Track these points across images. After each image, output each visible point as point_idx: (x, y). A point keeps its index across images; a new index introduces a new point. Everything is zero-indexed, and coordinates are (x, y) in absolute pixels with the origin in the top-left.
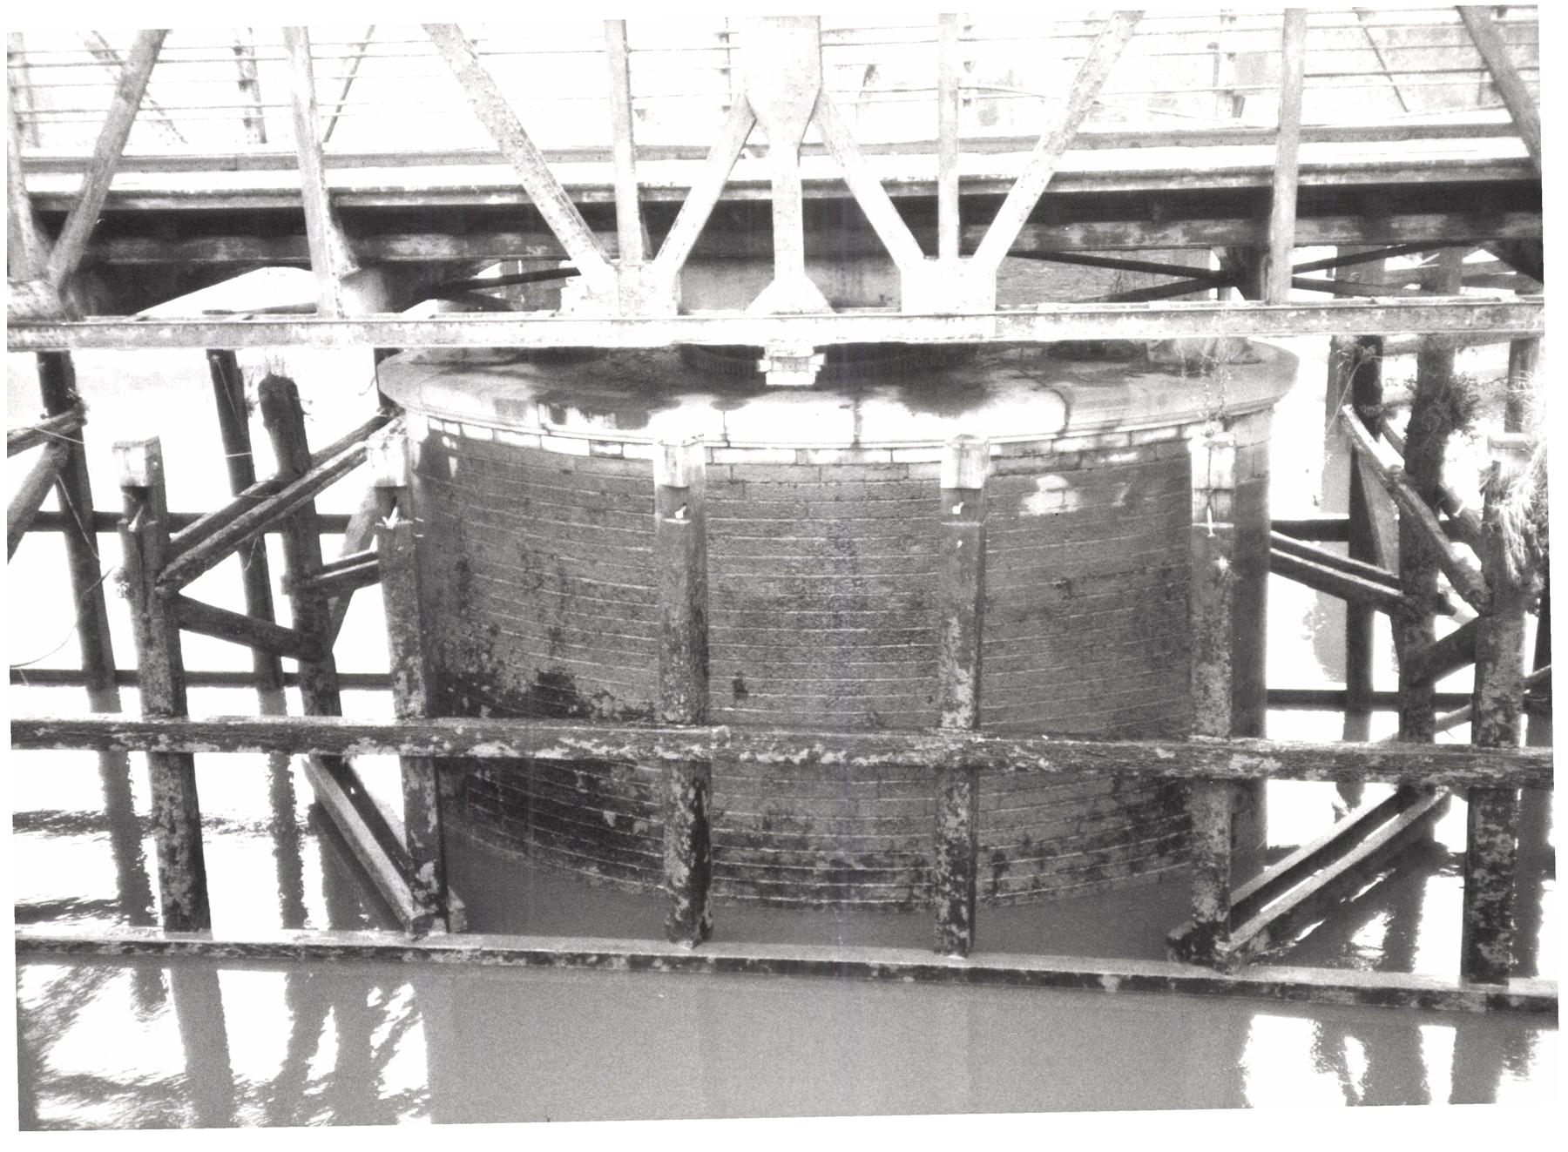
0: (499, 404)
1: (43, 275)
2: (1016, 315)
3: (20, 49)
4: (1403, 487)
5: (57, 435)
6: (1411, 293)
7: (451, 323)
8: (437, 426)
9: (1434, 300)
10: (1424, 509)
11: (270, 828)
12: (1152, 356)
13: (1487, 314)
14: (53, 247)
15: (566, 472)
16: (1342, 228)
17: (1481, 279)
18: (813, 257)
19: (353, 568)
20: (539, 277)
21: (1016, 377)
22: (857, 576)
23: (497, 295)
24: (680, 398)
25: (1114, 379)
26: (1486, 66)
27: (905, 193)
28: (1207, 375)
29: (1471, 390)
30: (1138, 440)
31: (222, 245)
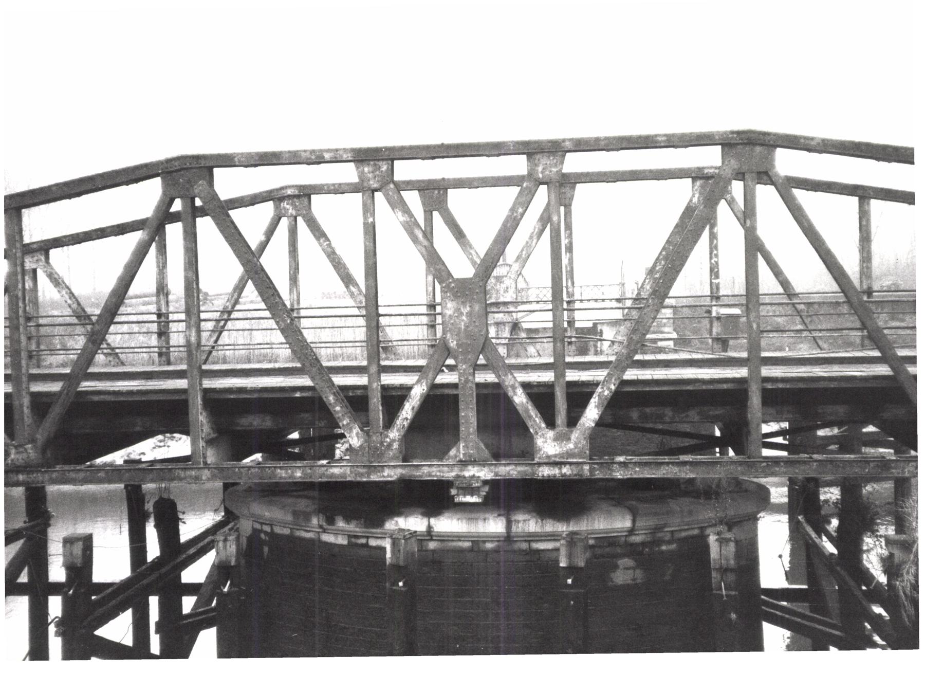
0: (295, 513)
1: (33, 441)
2: (602, 463)
3: (35, 315)
4: (838, 568)
5: (32, 533)
6: (832, 452)
7: (269, 467)
8: (258, 526)
9: (847, 456)
10: (852, 583)
11: (206, 446)
12: (683, 486)
13: (878, 466)
14: (41, 422)
15: (334, 556)
16: (788, 412)
17: (873, 441)
18: (482, 428)
19: (200, 617)
20: (322, 439)
21: (603, 499)
22: (510, 622)
23: (296, 451)
24: (403, 510)
25: (661, 499)
26: (864, 327)
27: (536, 390)
28: (716, 499)
29: (873, 509)
30: (677, 536)
31: (139, 421)
